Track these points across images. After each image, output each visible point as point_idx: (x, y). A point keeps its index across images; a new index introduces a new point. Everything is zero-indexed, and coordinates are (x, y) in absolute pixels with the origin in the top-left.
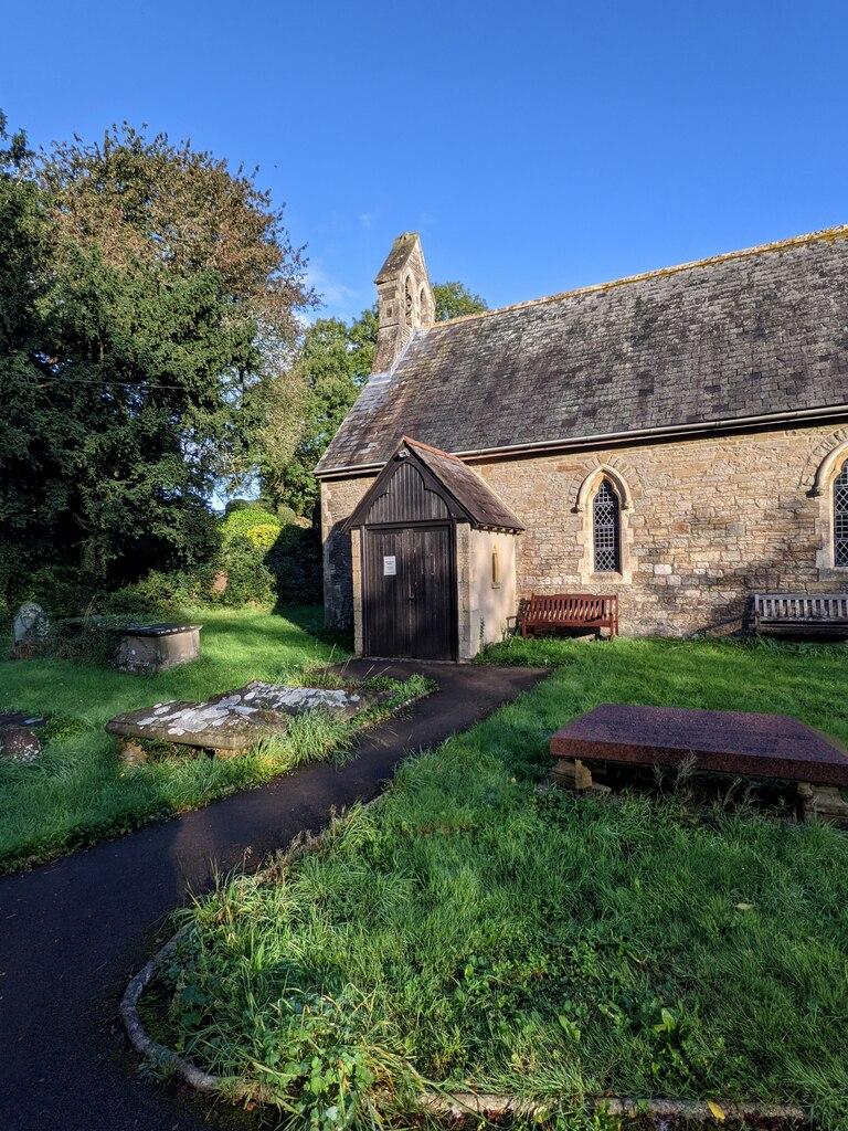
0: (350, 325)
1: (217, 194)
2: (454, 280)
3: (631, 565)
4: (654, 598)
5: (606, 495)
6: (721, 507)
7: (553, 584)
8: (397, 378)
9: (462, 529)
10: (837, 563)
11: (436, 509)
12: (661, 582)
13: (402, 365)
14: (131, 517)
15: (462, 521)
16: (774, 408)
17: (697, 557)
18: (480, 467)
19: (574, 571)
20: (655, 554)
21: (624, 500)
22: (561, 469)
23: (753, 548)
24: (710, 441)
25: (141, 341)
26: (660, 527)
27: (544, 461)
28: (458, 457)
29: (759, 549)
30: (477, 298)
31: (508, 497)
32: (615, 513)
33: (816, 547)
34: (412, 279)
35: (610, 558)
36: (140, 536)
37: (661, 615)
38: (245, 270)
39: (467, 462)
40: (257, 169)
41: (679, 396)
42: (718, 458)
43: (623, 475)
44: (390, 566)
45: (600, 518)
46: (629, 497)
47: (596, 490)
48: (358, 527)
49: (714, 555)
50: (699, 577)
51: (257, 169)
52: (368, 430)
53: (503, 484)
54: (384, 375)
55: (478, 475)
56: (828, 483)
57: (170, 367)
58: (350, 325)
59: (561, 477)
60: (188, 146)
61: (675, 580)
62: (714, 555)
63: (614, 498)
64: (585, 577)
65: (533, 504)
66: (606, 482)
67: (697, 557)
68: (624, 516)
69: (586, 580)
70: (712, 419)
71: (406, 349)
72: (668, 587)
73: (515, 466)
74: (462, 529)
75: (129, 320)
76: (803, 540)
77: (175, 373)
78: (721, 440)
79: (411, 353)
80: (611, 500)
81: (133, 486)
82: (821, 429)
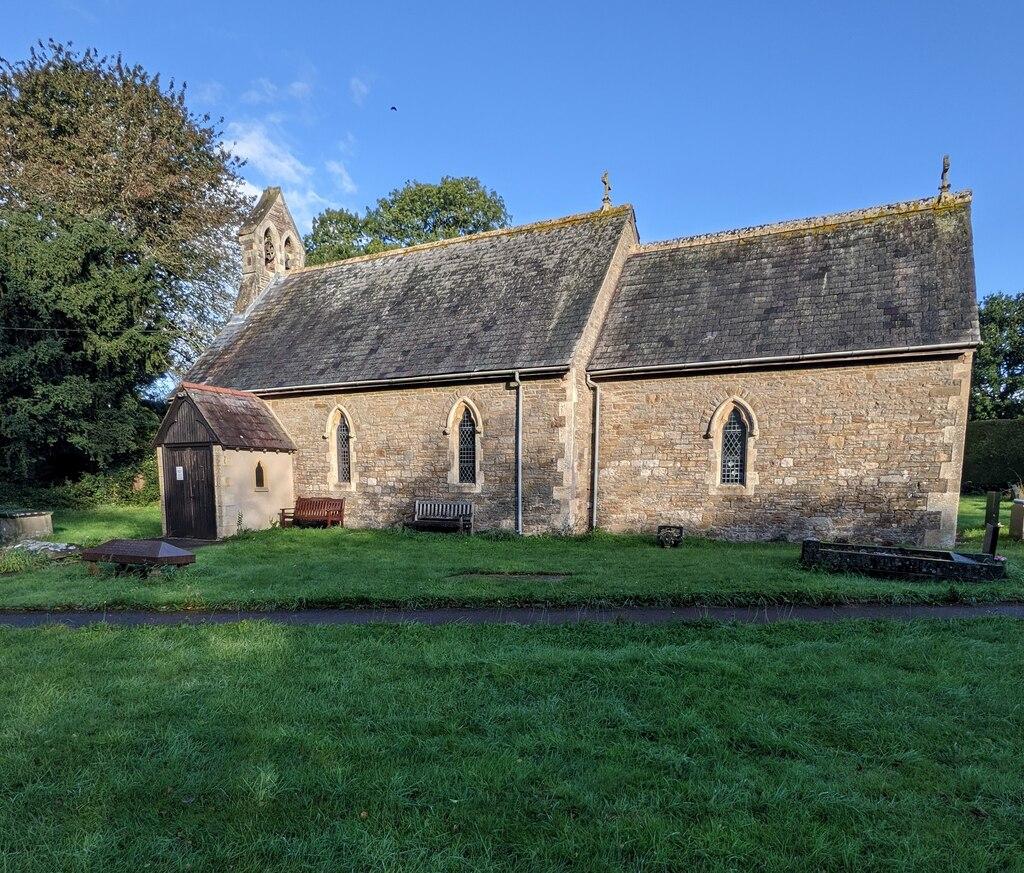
0: (362, 216)
1: (146, 104)
2: (458, 174)
3: (355, 478)
4: (368, 502)
5: (734, 424)
6: (400, 440)
7: (313, 490)
8: (250, 320)
9: (217, 449)
10: (461, 480)
11: (201, 436)
12: (370, 490)
13: (257, 308)
14: (41, 429)
15: (216, 443)
16: (422, 372)
17: (389, 474)
18: (271, 401)
19: (324, 481)
20: (366, 471)
21: (751, 424)
22: (317, 406)
23: (414, 470)
24: (394, 392)
25: (35, 284)
26: (369, 452)
27: (307, 400)
28: (254, 393)
29: (420, 469)
30: (494, 193)
31: (287, 427)
32: (743, 439)
33: (447, 469)
34: (274, 230)
35: (346, 476)
36: (54, 443)
37: (371, 513)
38: (175, 183)
39: (262, 397)
40: (185, 85)
41: (388, 360)
42: (399, 405)
43: (745, 399)
44: (180, 474)
45: (728, 449)
46: (756, 426)
47: (726, 418)
48: (160, 445)
49: (397, 473)
50: (390, 488)
51: (185, 85)
52: (212, 366)
53: (286, 415)
54: (241, 317)
55: (270, 408)
56: (453, 426)
57: (61, 306)
58: (362, 216)
59: (317, 412)
60: (119, 61)
61: (378, 490)
62: (397, 473)
63: (743, 426)
64: (330, 485)
65: (302, 431)
66: (735, 411)
67: (389, 474)
68: (751, 442)
69: (332, 488)
70: (392, 377)
71: (263, 293)
72: (375, 494)
73: (291, 402)
74: (217, 449)
75: (22, 267)
76: (440, 465)
77: (65, 311)
78: (400, 392)
79: (267, 298)
80: (739, 428)
81: (35, 403)
82: (450, 388)
